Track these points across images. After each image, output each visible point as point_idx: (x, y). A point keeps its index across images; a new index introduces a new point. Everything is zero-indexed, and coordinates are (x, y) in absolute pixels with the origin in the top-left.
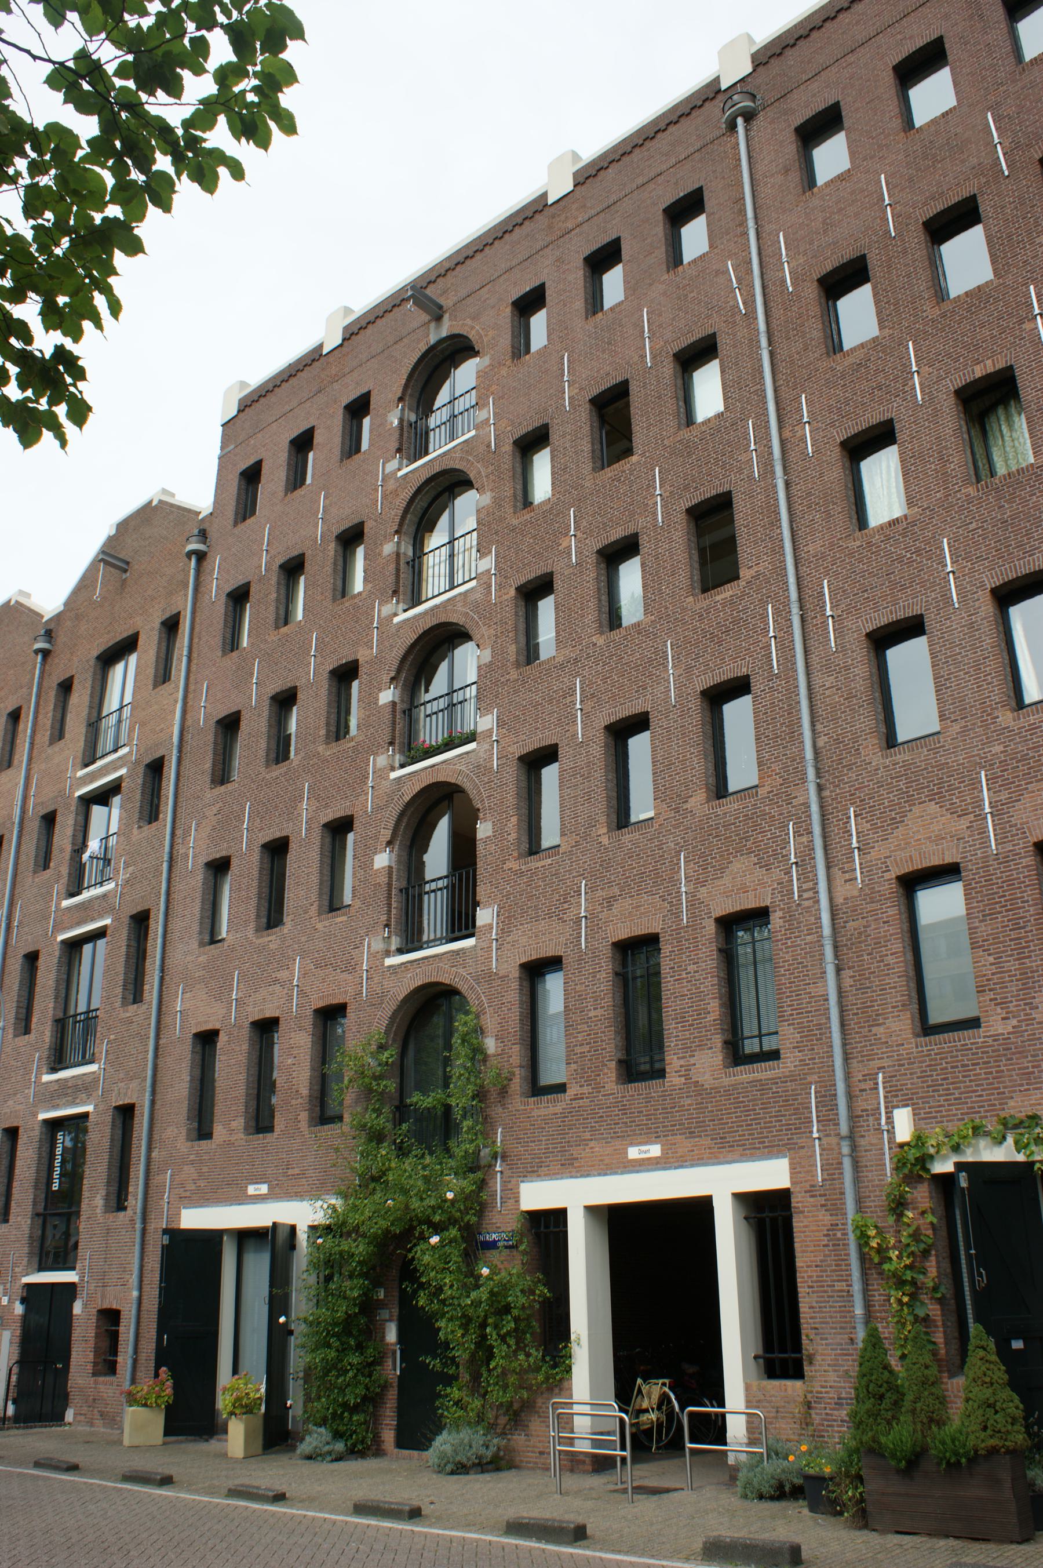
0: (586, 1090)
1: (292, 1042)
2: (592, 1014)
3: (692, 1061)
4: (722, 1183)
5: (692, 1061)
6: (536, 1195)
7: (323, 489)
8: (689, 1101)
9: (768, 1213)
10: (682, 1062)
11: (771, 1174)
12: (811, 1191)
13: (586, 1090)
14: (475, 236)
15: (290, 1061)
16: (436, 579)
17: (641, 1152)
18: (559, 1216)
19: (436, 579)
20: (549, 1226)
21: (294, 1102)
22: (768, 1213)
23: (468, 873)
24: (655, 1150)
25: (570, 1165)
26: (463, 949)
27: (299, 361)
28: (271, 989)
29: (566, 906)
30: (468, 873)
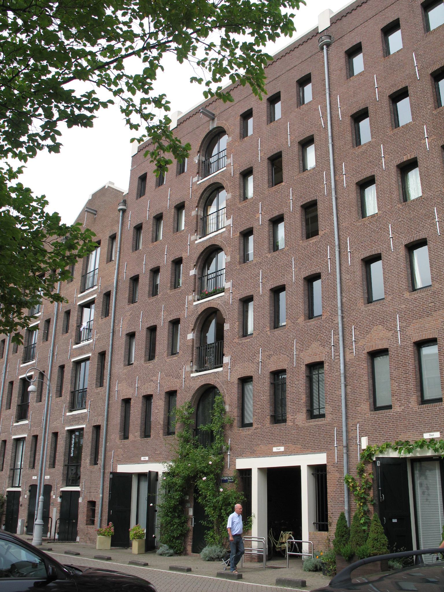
0: (260, 426)
4: (304, 461)
6: (242, 464)
11: (320, 459)
17: (277, 449)
20: (245, 475)
22: (319, 472)
24: (282, 449)
25: (253, 454)
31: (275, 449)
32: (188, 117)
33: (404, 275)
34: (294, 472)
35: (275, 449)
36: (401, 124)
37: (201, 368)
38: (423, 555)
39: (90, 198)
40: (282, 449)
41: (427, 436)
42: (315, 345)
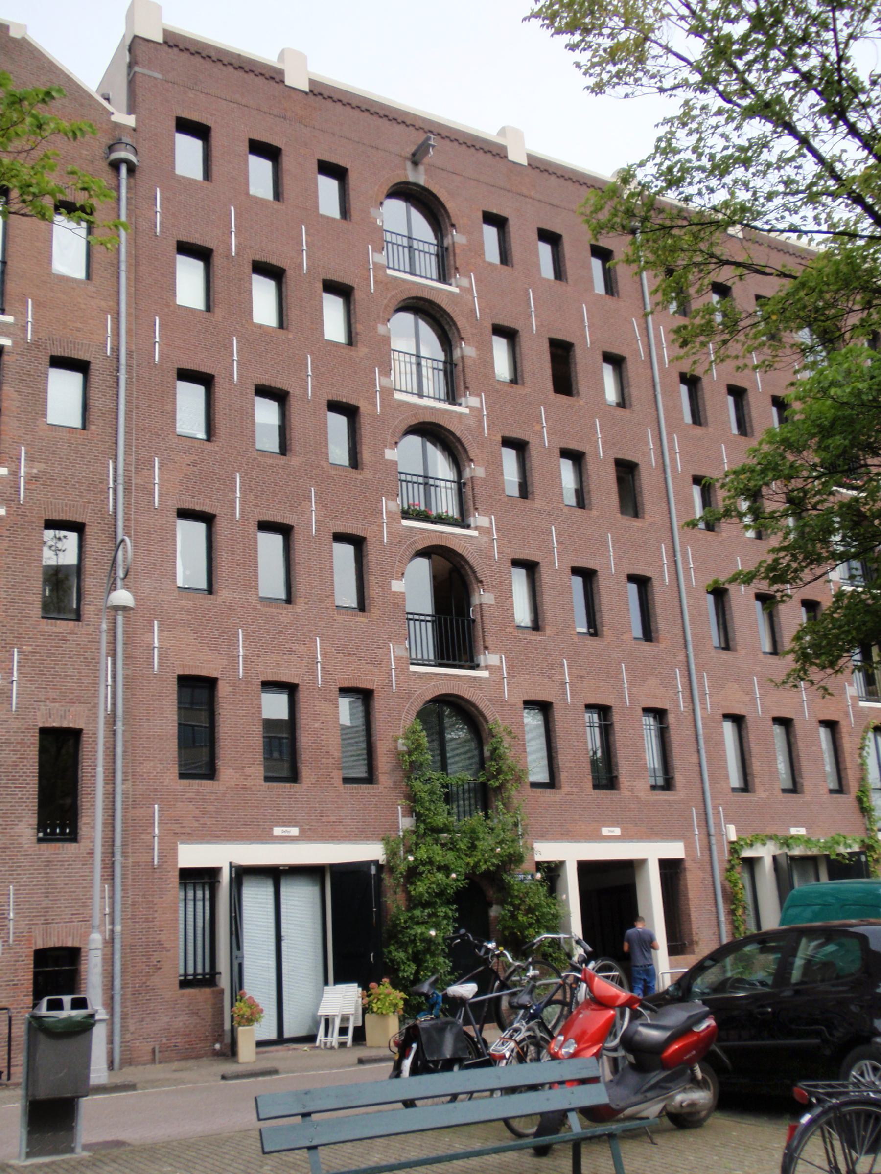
0: (575, 790)
1: (316, 708)
2: (575, 744)
3: (635, 784)
4: (651, 852)
5: (635, 784)
6: (546, 851)
7: (302, 222)
8: (633, 806)
9: (671, 870)
10: (629, 783)
11: (675, 850)
12: (694, 860)
13: (575, 790)
14: (442, 122)
15: (316, 725)
16: (403, 376)
17: (610, 831)
18: (561, 865)
19: (403, 376)
20: (552, 872)
21: (324, 760)
22: (671, 870)
23: (446, 620)
24: (617, 831)
25: (567, 835)
26: (479, 677)
27: (574, 171)
28: (285, 656)
29: (553, 671)
30: (446, 620)
31: (605, 831)
32: (364, 107)
33: (300, 570)
34: (629, 870)
35: (605, 831)
36: (256, 278)
37: (443, 659)
38: (549, 1027)
39: (13, 33)
40: (617, 831)
41: (794, 831)
42: (652, 682)
